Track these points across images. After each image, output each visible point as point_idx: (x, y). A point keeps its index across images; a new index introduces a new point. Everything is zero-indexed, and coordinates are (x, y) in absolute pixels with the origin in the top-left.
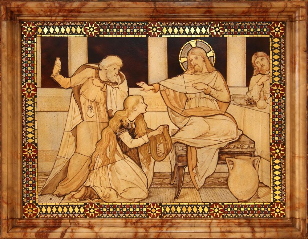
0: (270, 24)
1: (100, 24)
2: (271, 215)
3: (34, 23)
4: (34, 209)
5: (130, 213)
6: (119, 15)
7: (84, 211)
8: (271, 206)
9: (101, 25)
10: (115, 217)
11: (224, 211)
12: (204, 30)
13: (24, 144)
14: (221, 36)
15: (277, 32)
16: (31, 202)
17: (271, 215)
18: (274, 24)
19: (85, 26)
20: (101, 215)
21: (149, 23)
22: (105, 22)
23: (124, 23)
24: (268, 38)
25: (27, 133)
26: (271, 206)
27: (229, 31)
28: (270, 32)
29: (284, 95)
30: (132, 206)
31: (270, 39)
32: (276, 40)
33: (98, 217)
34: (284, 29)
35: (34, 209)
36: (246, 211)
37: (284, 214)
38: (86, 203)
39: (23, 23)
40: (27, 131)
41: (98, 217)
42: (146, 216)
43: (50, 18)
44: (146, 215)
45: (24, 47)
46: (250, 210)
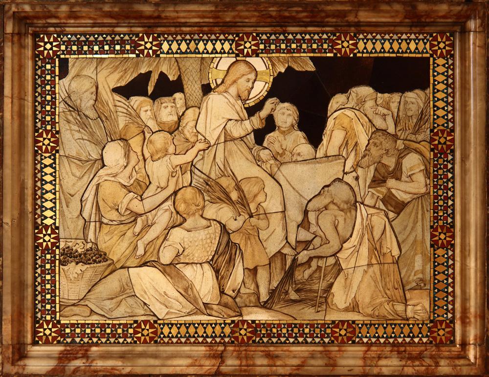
0: (136, 37)
1: (61, 39)
2: (135, 339)
3: (156, 35)
4: (143, 327)
5: (117, 336)
6: (443, 26)
7: (231, 333)
8: (135, 325)
9: (63, 39)
10: (110, 343)
11: (254, 332)
12: (421, 46)
13: (37, 228)
14: (352, 55)
15: (52, 46)
16: (48, 318)
17: (135, 339)
18: (436, 36)
19: (432, 40)
20: (62, 339)
21: (338, 34)
22: (168, 35)
23: (371, 35)
24: (428, 59)
25: (44, 209)
26: (135, 325)
27: (91, 47)
28: (333, 48)
29: (452, 147)
30: (90, 326)
31: (431, 59)
32: (441, 61)
33: (59, 342)
34: (452, 45)
35: (143, 327)
36: (269, 333)
37: (452, 339)
38: (137, 321)
39: (451, 35)
40: (44, 207)
41: (59, 342)
42: (132, 342)
43: (111, 29)
44: (133, 339)
45: (449, 74)
46: (110, 332)
